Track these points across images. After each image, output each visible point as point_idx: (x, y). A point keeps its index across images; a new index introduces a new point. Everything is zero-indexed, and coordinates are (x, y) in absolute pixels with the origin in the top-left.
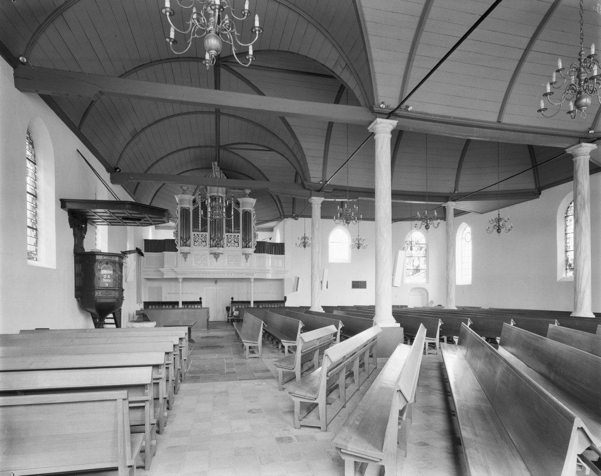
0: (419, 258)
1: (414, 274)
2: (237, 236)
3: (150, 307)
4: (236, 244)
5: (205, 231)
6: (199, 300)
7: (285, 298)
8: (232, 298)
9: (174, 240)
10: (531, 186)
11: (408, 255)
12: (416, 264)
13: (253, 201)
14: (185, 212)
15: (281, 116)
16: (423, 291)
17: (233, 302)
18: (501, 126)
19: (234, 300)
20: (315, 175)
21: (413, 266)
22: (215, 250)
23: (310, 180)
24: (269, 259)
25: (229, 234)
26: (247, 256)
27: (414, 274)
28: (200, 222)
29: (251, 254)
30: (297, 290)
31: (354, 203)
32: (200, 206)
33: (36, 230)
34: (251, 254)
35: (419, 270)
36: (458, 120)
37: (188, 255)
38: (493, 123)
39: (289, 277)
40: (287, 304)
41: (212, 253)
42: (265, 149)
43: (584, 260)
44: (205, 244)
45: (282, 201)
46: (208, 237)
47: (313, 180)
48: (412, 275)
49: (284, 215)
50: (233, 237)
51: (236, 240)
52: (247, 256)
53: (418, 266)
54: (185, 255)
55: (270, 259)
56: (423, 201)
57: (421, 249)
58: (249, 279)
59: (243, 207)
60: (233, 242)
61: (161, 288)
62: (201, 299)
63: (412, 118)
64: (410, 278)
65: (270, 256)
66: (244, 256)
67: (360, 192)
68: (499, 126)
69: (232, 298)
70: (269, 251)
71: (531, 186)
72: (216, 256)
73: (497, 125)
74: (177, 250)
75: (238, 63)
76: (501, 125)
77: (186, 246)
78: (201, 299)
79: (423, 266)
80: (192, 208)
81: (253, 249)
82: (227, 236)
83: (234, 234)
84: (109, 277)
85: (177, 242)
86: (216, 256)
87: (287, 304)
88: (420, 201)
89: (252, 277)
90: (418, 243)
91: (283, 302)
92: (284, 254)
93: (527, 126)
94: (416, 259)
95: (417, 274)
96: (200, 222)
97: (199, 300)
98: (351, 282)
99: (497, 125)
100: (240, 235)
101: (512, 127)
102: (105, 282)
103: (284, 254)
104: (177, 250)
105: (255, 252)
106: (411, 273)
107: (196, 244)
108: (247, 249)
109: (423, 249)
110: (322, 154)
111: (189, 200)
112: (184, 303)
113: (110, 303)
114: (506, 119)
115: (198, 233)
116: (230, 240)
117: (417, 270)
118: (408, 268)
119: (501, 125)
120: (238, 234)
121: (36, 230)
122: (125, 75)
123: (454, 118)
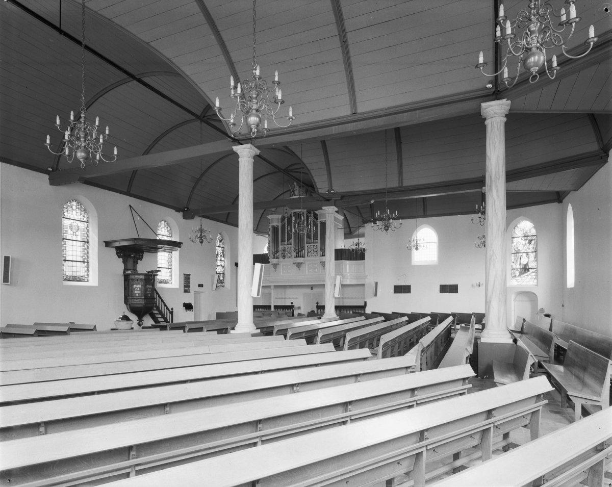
0: (527, 254)
1: (521, 274)
7: (365, 303)
8: (317, 303)
10: (593, 147)
11: (514, 252)
12: (524, 261)
14: (275, 229)
15: (284, 145)
16: (530, 296)
18: (357, 117)
20: (322, 187)
21: (520, 264)
22: (300, 260)
23: (318, 191)
27: (521, 274)
28: (286, 236)
30: (376, 295)
31: (459, 198)
33: (88, 262)
35: (528, 270)
36: (324, 123)
37: (278, 266)
38: (348, 116)
39: (370, 281)
41: (295, 263)
43: (490, 259)
46: (292, 249)
47: (320, 191)
48: (519, 276)
51: (315, 250)
53: (527, 264)
55: (348, 265)
56: (435, 193)
57: (530, 242)
59: (320, 219)
60: (312, 251)
61: (270, 294)
62: (292, 303)
63: (369, 119)
64: (517, 280)
65: (348, 262)
67: (372, 194)
68: (356, 117)
71: (593, 147)
72: (299, 265)
73: (353, 117)
74: (269, 262)
75: (571, 59)
76: (357, 117)
78: (292, 303)
79: (532, 265)
80: (280, 225)
83: (314, 244)
84: (138, 289)
86: (299, 265)
88: (457, 194)
89: (272, 284)
90: (526, 235)
93: (389, 108)
94: (524, 255)
95: (526, 274)
96: (286, 236)
98: (393, 287)
99: (353, 117)
100: (319, 245)
101: (371, 115)
102: (136, 293)
106: (517, 273)
108: (299, 258)
109: (533, 242)
110: (324, 165)
112: (276, 307)
113: (139, 307)
114: (362, 109)
115: (310, 245)
116: (310, 250)
117: (525, 269)
118: (514, 267)
119: (357, 117)
120: (291, 246)
121: (88, 262)
122: (147, 152)
123: (302, 125)
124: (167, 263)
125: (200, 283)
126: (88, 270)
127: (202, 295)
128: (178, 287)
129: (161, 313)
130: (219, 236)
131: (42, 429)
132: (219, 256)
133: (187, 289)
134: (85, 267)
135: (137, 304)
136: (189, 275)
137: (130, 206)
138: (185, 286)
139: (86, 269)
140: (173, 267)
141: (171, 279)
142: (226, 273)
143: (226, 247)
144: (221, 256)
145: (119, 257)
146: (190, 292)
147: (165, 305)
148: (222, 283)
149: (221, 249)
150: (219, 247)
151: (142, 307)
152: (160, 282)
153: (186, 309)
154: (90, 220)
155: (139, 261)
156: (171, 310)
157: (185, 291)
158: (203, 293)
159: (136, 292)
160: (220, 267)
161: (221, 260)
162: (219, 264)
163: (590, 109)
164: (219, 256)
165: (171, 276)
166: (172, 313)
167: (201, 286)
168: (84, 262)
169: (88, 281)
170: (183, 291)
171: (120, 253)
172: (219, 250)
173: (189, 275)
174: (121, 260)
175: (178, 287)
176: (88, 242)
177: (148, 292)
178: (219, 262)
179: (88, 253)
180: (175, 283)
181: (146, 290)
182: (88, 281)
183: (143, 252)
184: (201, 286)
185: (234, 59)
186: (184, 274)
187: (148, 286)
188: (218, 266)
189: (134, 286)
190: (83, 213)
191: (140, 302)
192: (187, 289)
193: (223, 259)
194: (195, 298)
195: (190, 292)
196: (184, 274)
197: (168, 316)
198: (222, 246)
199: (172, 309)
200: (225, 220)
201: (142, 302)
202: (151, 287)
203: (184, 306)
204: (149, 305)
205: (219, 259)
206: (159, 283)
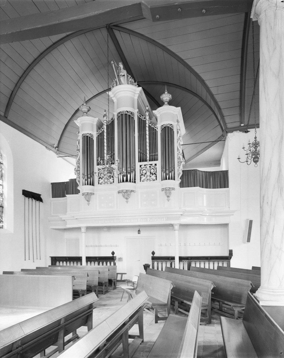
2: (153, 165)
3: (58, 263)
4: (153, 177)
5: (154, 158)
6: (112, 255)
7: (231, 252)
8: (153, 253)
9: (75, 179)
13: (177, 111)
14: (88, 140)
17: (154, 258)
19: (155, 255)
24: (201, 196)
25: (143, 163)
26: (168, 191)
29: (173, 189)
32: (105, 131)
34: (173, 189)
40: (234, 263)
42: (55, 38)
44: (155, 178)
45: (222, 107)
46: (159, 167)
49: (227, 128)
50: (148, 166)
51: (152, 171)
52: (168, 191)
54: (88, 196)
58: (172, 225)
60: (148, 173)
62: (113, 253)
66: (121, 194)
69: (153, 253)
70: (201, 185)
72: (126, 194)
74: (77, 192)
77: (127, 181)
78: (113, 253)
81: (178, 181)
82: (141, 166)
85: (79, 181)
86: (126, 194)
87: (234, 263)
91: (227, 259)
92: (228, 187)
97: (112, 255)
103: (228, 187)
104: (77, 192)
105: (182, 185)
107: (101, 181)
111: (92, 125)
116: (144, 172)
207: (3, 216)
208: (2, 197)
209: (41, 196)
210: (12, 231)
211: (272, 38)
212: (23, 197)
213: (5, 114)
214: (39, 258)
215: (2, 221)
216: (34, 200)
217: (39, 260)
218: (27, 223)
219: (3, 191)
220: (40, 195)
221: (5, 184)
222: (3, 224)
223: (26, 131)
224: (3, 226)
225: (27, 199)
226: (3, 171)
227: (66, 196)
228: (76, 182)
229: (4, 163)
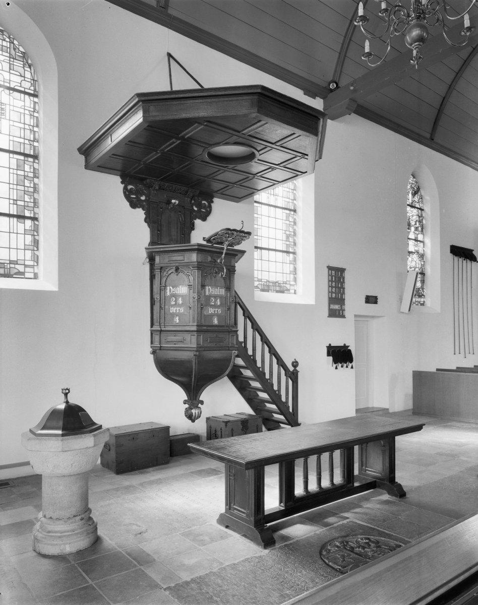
33: (34, 219)
84: (180, 301)
102: (173, 315)
121: (34, 219)
124: (281, 235)
125: (458, 366)
126: (36, 243)
127: (374, 323)
128: (312, 301)
129: (259, 375)
130: (411, 180)
131: (318, 476)
132: (413, 229)
133: (337, 307)
134: (26, 232)
135: (176, 349)
136: (342, 270)
137: (170, 55)
138: (331, 301)
139: (29, 239)
140: (299, 250)
141: (295, 280)
142: (428, 271)
143: (427, 208)
144: (416, 229)
145: (134, 205)
146: (343, 316)
147: (273, 352)
148: (420, 296)
149: (415, 211)
150: (412, 206)
151: (190, 362)
152: (266, 289)
153: (335, 361)
154: (41, 91)
155: (198, 222)
156: (291, 369)
157: (333, 314)
158: (375, 321)
159: (173, 310)
160: (415, 256)
161: (416, 240)
162: (411, 248)
163: (367, 444)
164: (413, 229)
165: (295, 271)
166: (293, 376)
167: (371, 300)
168: (21, 217)
169: (36, 277)
170: (326, 313)
171: (138, 193)
172: (412, 213)
173: (342, 270)
174: (140, 213)
175: (312, 301)
176: (35, 157)
177: (211, 311)
178: (411, 243)
179: (36, 189)
180: (307, 290)
181: (203, 302)
182: (36, 277)
183: (212, 197)
184: (371, 300)
185: (453, 76)
186: (330, 268)
187: (209, 290)
188: (410, 253)
189: (169, 291)
190: (18, 64)
191: (187, 346)
192: (337, 307)
193: (420, 237)
194: (359, 335)
195: (343, 316)
196: (330, 268)
197: (283, 385)
198: (417, 206)
199: (295, 364)
200: (428, 136)
201: (192, 342)
202: (222, 292)
203: (329, 355)
204: (216, 355)
205: (412, 236)
206: (263, 290)
207: (425, 287)
208: (423, 259)
209: (474, 252)
210: (438, 309)
211: (410, 480)
212: (451, 256)
213: (431, 134)
214: (472, 352)
215: (423, 295)
216: (468, 261)
217: (471, 355)
218: (456, 299)
219: (424, 250)
220: (472, 250)
221: (428, 241)
222: (425, 300)
223: (446, 148)
224: (424, 302)
225: (456, 258)
226: (424, 222)
227: (243, 252)
228: (173, 137)
229: (425, 208)
